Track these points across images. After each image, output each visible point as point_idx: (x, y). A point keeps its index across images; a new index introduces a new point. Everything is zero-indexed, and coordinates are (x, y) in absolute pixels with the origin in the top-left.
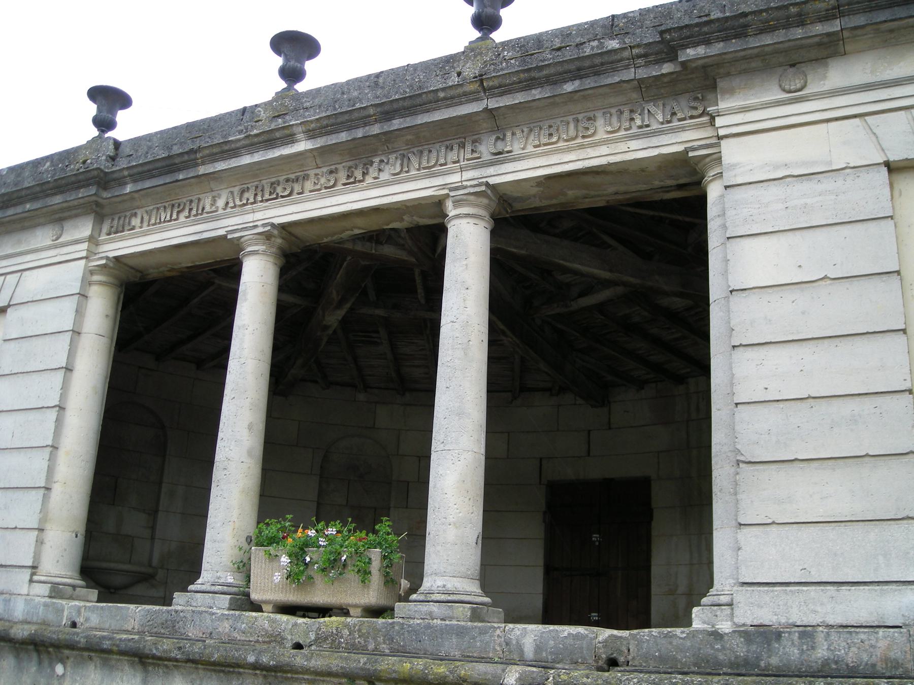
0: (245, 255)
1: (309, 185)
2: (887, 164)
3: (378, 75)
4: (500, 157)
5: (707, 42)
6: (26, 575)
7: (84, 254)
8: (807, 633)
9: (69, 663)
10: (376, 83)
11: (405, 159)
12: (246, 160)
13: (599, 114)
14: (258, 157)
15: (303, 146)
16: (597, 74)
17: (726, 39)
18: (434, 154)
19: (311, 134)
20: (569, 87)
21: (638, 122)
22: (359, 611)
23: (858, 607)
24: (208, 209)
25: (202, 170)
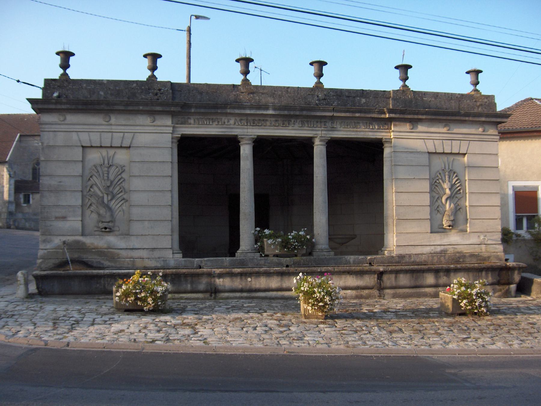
0: (242, 145)
1: (268, 123)
2: (428, 152)
3: (288, 88)
4: (333, 129)
5: (395, 113)
6: (171, 252)
7: (171, 132)
8: (410, 255)
9: (253, 278)
10: (288, 91)
11: (303, 123)
12: (248, 112)
13: (361, 122)
14: (253, 112)
15: (271, 112)
16: (365, 113)
17: (400, 114)
18: (312, 123)
19: (275, 109)
20: (357, 115)
21: (371, 127)
22: (270, 256)
23: (418, 250)
24: (226, 123)
25: (229, 111)
